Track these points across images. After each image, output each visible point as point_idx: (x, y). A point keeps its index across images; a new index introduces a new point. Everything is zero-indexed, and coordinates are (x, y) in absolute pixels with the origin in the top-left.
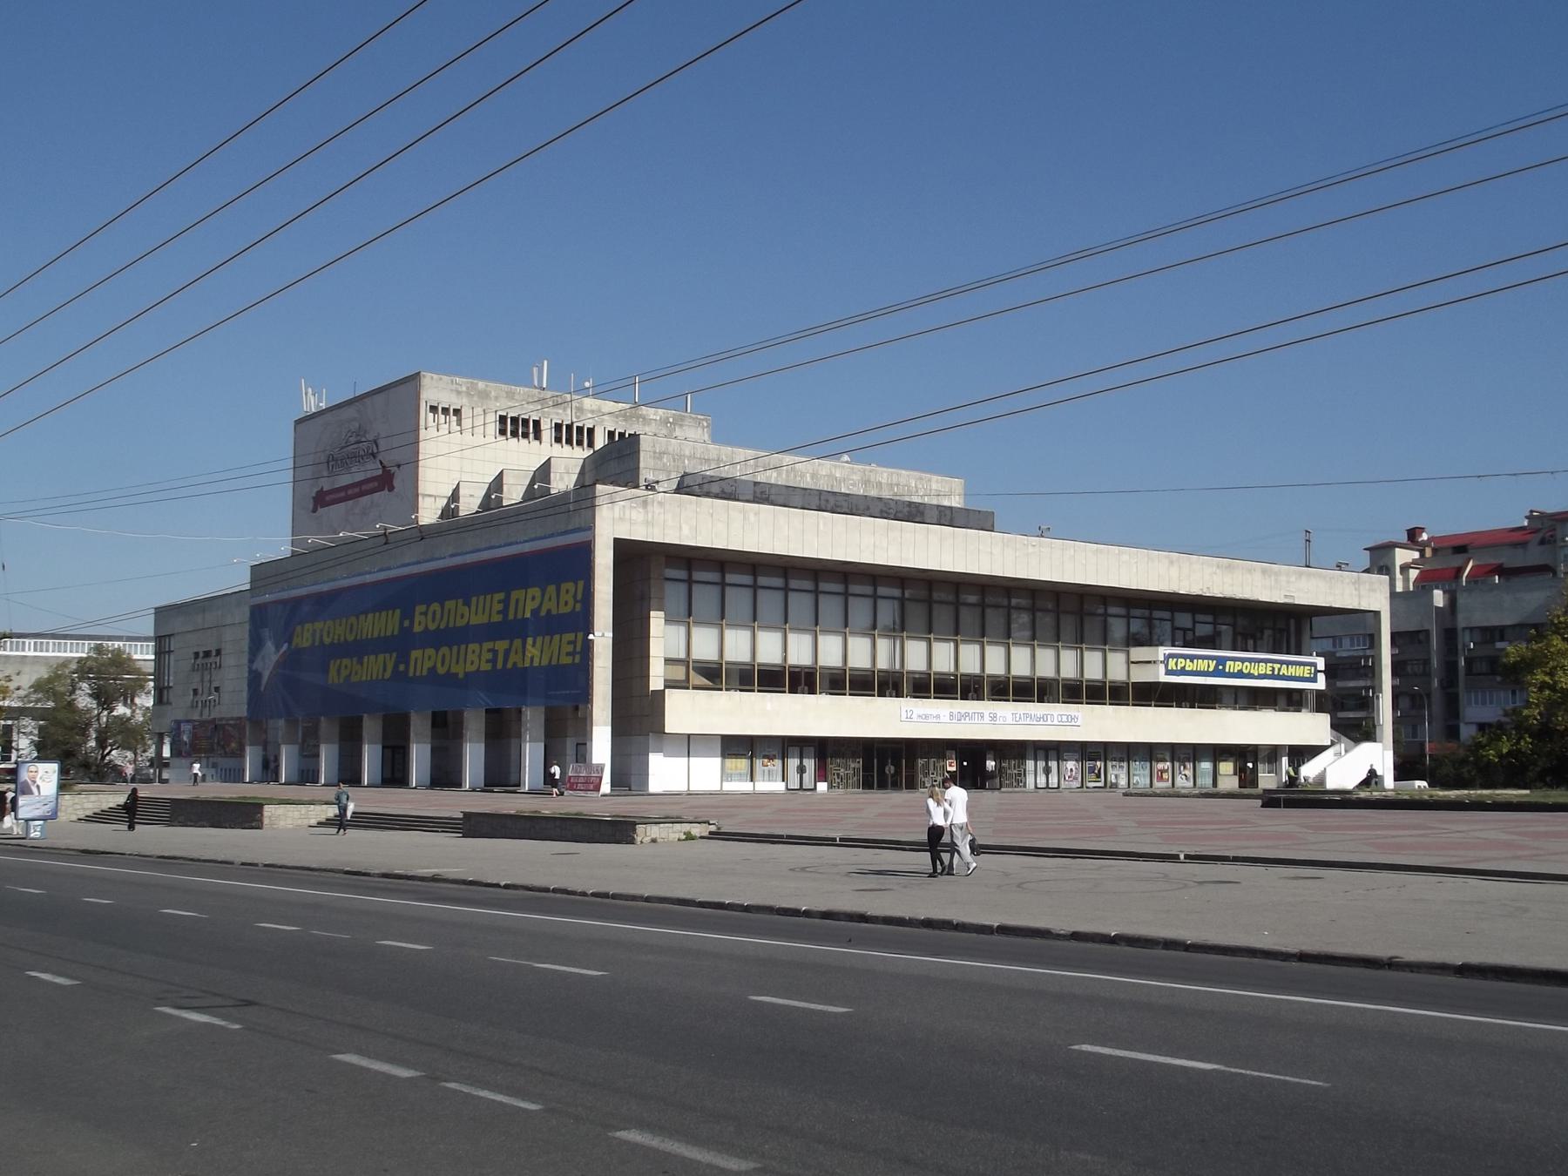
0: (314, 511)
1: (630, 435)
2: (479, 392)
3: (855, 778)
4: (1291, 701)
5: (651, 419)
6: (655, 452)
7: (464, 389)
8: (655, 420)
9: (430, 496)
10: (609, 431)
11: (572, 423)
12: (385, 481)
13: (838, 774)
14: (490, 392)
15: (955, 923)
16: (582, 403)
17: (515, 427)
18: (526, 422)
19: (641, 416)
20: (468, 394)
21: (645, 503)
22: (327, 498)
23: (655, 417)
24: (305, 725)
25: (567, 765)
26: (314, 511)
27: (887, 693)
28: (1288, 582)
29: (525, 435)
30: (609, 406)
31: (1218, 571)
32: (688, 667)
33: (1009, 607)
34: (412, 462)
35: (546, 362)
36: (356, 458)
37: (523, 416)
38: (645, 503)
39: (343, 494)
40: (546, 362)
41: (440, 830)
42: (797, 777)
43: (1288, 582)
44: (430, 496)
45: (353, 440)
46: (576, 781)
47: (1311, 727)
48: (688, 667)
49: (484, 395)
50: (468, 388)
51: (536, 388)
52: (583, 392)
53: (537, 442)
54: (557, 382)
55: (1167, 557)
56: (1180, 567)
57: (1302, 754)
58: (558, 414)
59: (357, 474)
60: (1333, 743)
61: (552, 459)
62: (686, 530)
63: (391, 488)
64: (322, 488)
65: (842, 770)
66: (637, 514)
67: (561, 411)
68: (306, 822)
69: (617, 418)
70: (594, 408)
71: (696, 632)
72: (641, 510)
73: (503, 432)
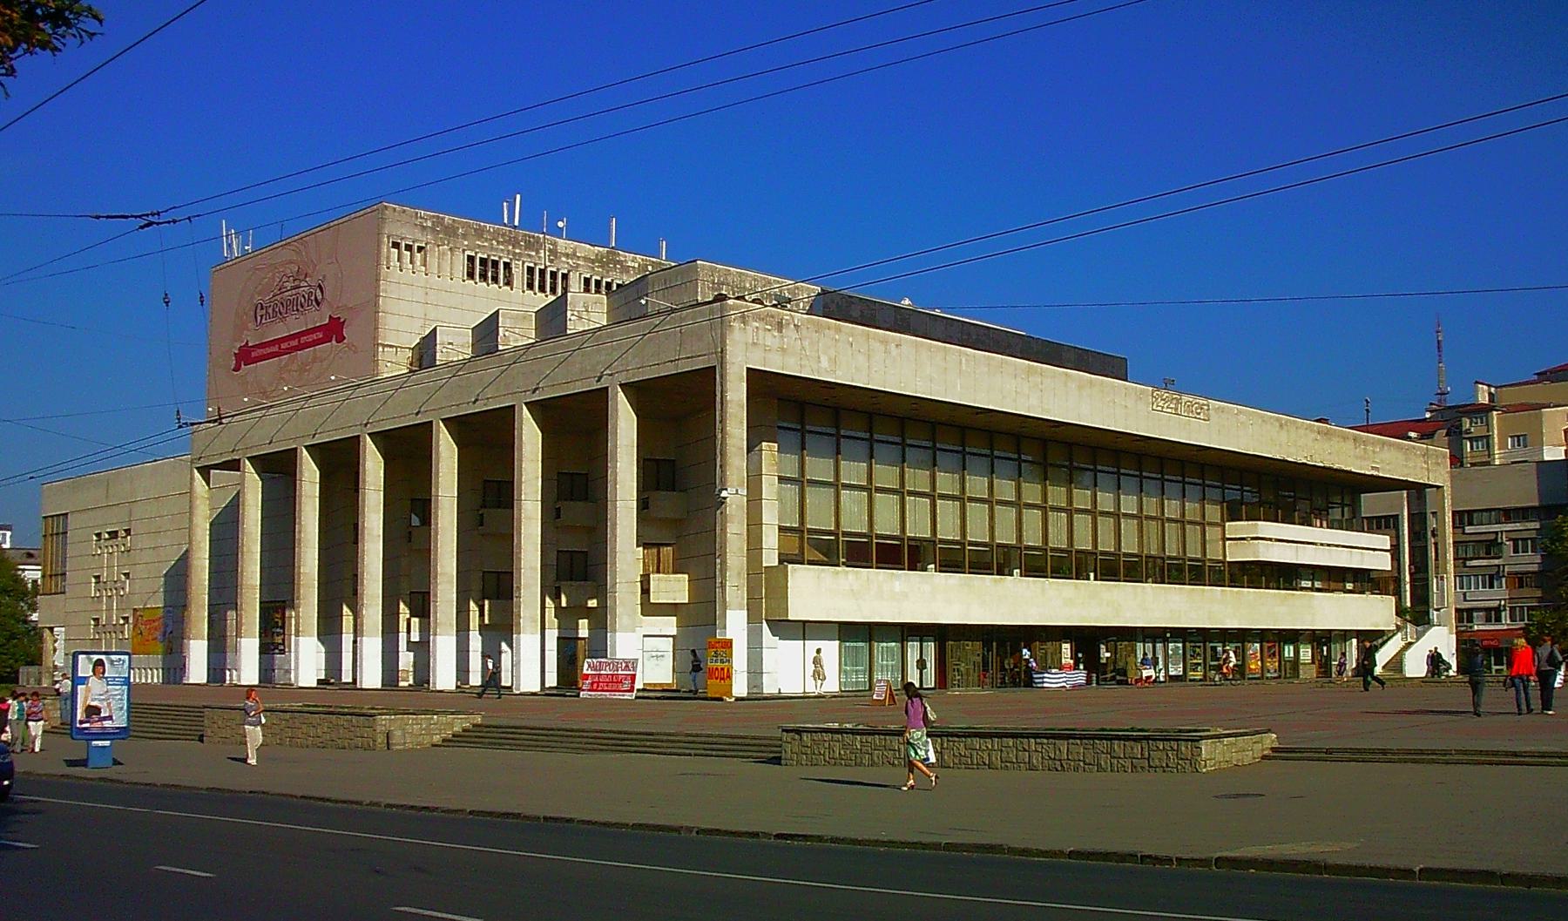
0: (237, 369)
1: (618, 285)
2: (446, 227)
3: (976, 674)
4: (1363, 581)
5: (629, 266)
6: (713, 283)
7: (430, 224)
8: (634, 267)
9: (391, 346)
10: (585, 278)
11: (546, 267)
12: (333, 330)
13: (958, 670)
14: (458, 228)
15: (1368, 866)
16: (555, 244)
17: (485, 270)
18: (495, 264)
19: (620, 262)
20: (433, 229)
21: (780, 326)
22: (253, 354)
23: (633, 264)
24: (1375, 527)
25: (580, 663)
26: (237, 369)
27: (1006, 571)
28: (1374, 452)
29: (495, 280)
30: (586, 249)
31: (1319, 437)
32: (801, 539)
33: (1119, 474)
34: (371, 307)
35: (518, 197)
36: (295, 306)
37: (492, 258)
38: (780, 326)
39: (275, 349)
40: (518, 197)
41: (693, 752)
42: (917, 673)
43: (1374, 452)
44: (391, 346)
45: (289, 285)
46: (596, 680)
47: (1375, 611)
48: (801, 539)
49: (450, 231)
50: (433, 224)
51: (505, 225)
52: (558, 233)
53: (508, 288)
54: (531, 220)
55: (1278, 420)
56: (1288, 431)
57: (1371, 640)
58: (530, 256)
59: (295, 324)
60: (1399, 628)
61: (501, 311)
62: (825, 363)
63: (341, 339)
64: (247, 343)
65: (963, 665)
66: (771, 339)
67: (533, 253)
68: (427, 740)
69: (593, 264)
70: (570, 251)
71: (940, 475)
72: (776, 334)
73: (471, 275)
